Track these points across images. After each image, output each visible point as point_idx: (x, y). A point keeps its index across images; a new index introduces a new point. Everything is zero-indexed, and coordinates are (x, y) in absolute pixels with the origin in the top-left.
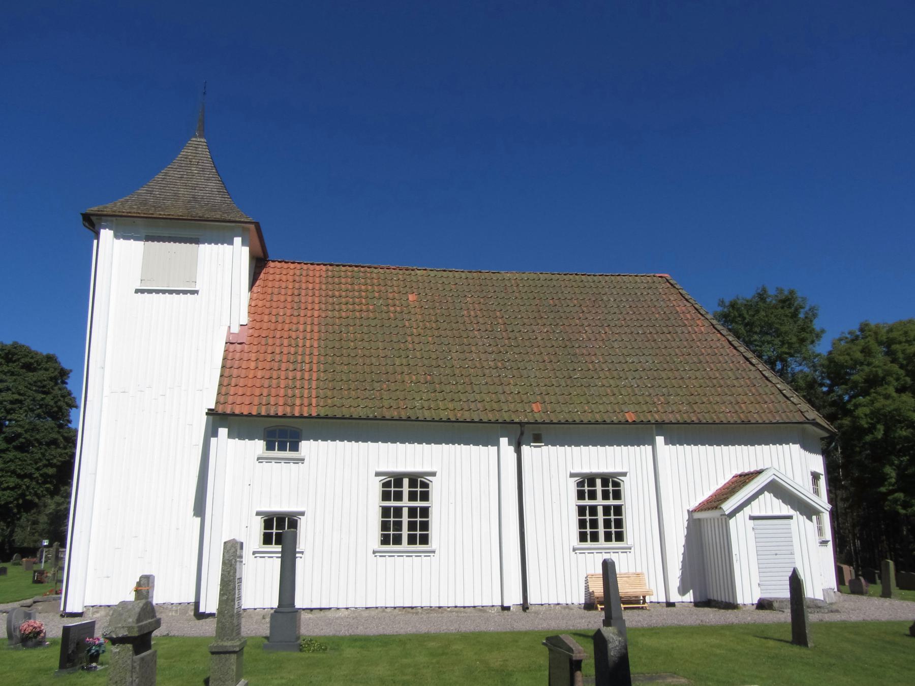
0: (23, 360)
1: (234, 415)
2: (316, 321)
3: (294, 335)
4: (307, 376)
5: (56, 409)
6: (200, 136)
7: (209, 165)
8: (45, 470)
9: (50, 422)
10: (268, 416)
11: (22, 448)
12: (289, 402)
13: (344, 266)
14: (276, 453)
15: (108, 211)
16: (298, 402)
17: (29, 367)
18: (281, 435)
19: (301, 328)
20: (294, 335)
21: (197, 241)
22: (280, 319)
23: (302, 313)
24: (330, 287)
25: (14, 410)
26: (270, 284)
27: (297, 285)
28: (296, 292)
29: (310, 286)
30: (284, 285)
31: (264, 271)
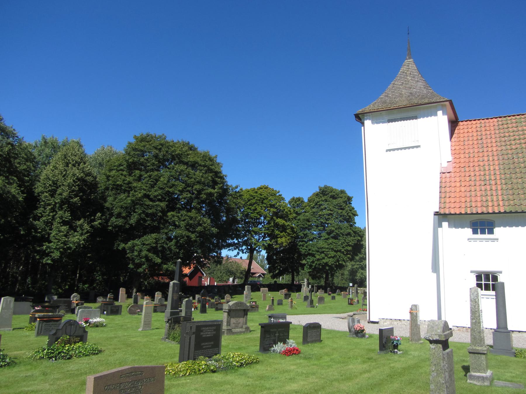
0: (330, 194)
1: (451, 214)
2: (495, 153)
3: (481, 164)
4: (494, 188)
5: (348, 217)
6: (410, 58)
7: (416, 73)
8: (346, 248)
9: (346, 224)
10: (472, 214)
11: (335, 238)
12: (485, 204)
13: (509, 116)
14: (479, 236)
15: (367, 110)
16: (490, 204)
17: (333, 197)
18: (483, 224)
19: (486, 159)
20: (481, 164)
21: (416, 118)
22: (471, 155)
23: (485, 150)
24: (502, 131)
25: (329, 218)
26: (462, 135)
27: (479, 133)
28: (479, 138)
29: (488, 133)
30: (470, 135)
31: (457, 128)
